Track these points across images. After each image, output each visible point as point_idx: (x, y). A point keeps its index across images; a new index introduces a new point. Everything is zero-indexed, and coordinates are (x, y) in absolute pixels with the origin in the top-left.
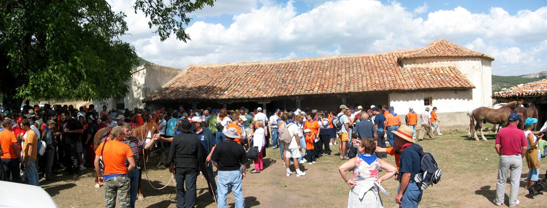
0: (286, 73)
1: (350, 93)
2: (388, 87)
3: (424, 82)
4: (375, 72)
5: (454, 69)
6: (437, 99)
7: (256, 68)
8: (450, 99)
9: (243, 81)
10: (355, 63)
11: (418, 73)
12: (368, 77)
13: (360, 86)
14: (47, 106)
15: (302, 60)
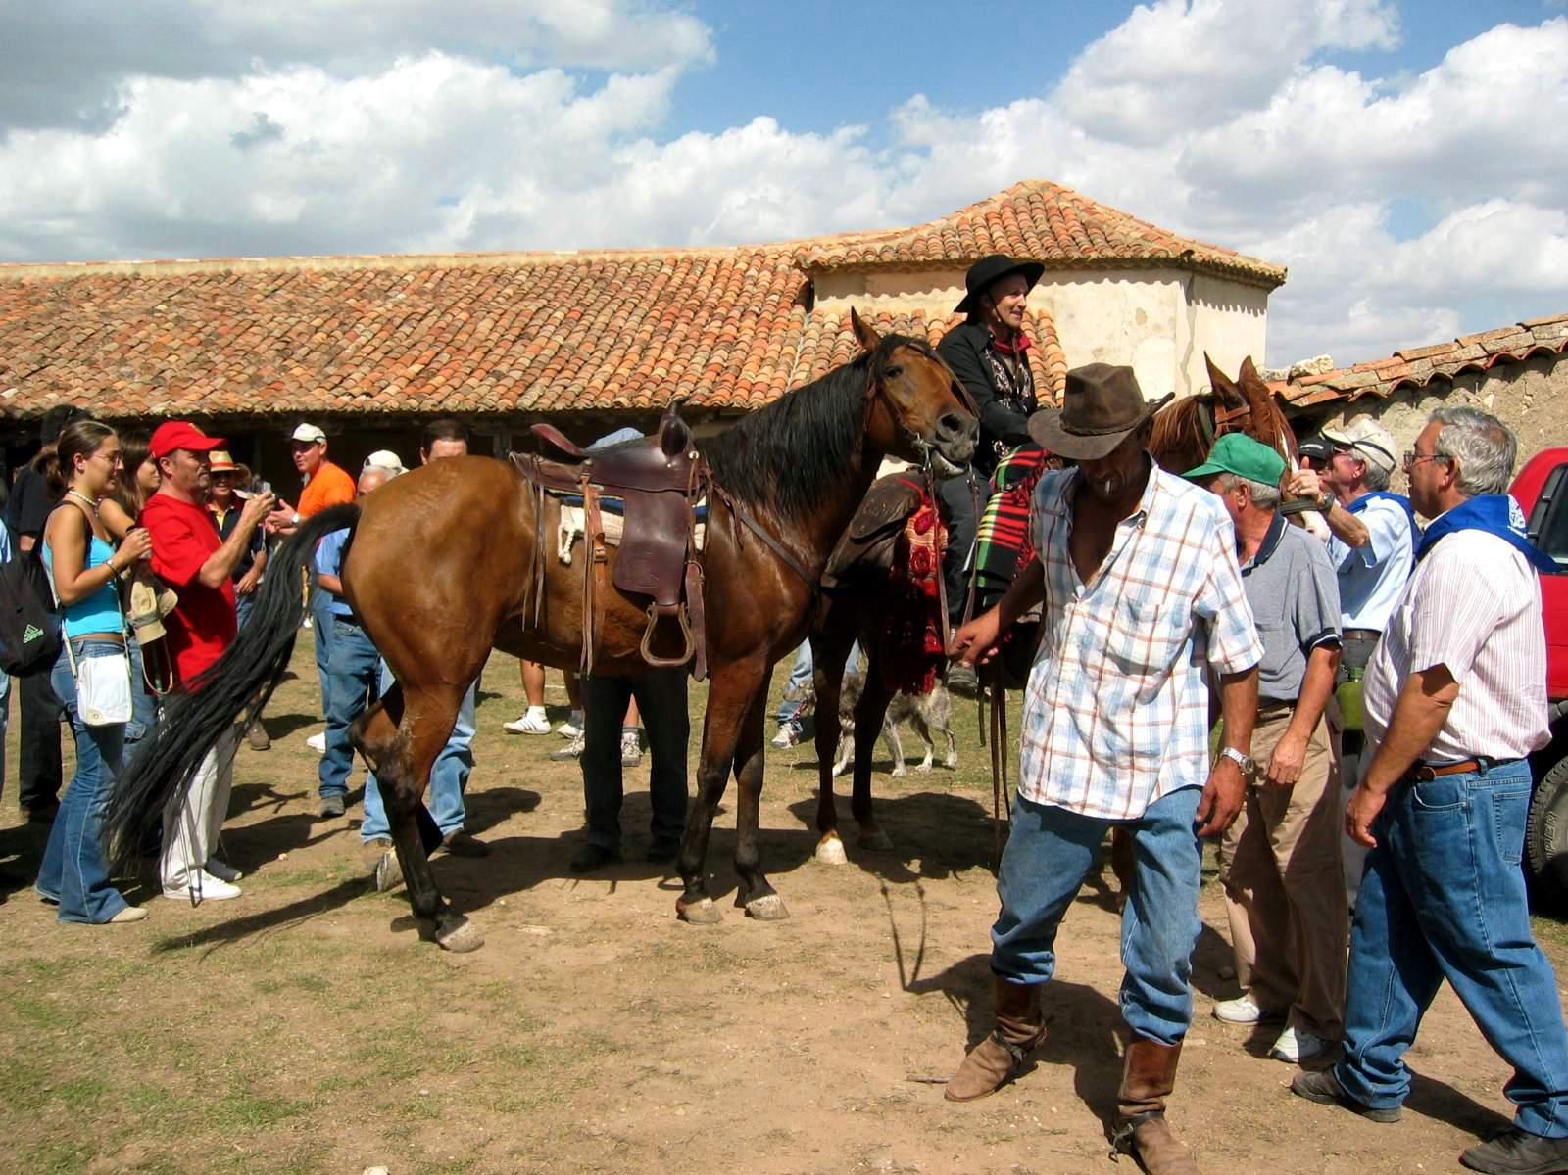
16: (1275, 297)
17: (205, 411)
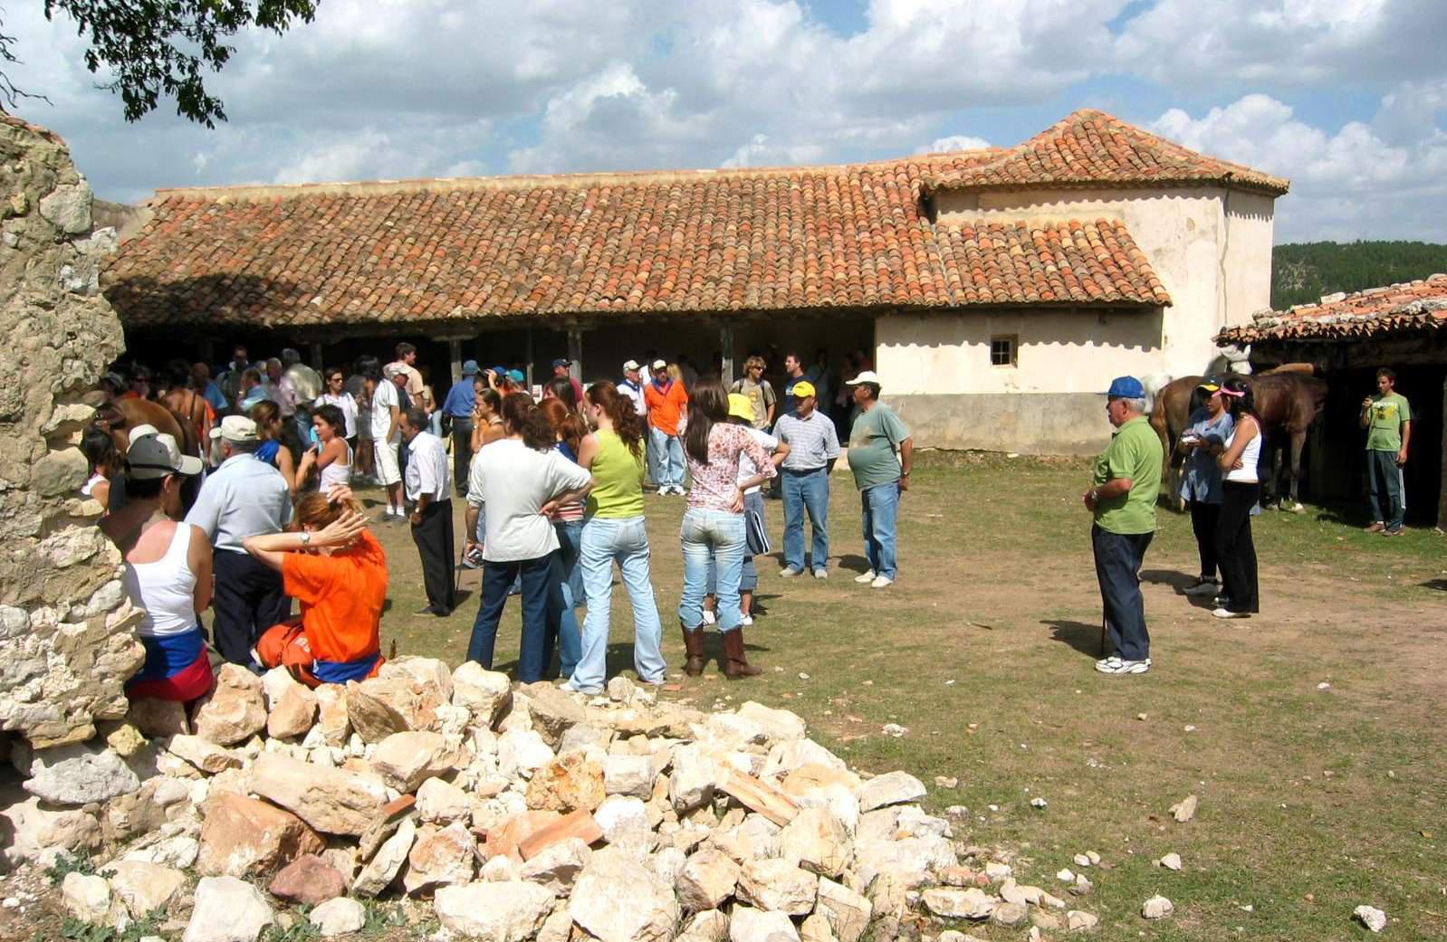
0: (533, 230)
1: (745, 312)
2: (870, 295)
3: (996, 281)
4: (837, 237)
5: (1115, 231)
6: (1034, 343)
7: (415, 205)
8: (1081, 343)
9: (374, 259)
10: (773, 202)
11: (985, 243)
12: (811, 256)
13: (782, 290)
14: (151, 290)
15: (590, 181)
16: (1279, 202)
17: (498, 314)
